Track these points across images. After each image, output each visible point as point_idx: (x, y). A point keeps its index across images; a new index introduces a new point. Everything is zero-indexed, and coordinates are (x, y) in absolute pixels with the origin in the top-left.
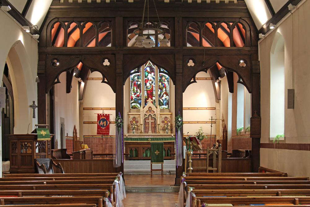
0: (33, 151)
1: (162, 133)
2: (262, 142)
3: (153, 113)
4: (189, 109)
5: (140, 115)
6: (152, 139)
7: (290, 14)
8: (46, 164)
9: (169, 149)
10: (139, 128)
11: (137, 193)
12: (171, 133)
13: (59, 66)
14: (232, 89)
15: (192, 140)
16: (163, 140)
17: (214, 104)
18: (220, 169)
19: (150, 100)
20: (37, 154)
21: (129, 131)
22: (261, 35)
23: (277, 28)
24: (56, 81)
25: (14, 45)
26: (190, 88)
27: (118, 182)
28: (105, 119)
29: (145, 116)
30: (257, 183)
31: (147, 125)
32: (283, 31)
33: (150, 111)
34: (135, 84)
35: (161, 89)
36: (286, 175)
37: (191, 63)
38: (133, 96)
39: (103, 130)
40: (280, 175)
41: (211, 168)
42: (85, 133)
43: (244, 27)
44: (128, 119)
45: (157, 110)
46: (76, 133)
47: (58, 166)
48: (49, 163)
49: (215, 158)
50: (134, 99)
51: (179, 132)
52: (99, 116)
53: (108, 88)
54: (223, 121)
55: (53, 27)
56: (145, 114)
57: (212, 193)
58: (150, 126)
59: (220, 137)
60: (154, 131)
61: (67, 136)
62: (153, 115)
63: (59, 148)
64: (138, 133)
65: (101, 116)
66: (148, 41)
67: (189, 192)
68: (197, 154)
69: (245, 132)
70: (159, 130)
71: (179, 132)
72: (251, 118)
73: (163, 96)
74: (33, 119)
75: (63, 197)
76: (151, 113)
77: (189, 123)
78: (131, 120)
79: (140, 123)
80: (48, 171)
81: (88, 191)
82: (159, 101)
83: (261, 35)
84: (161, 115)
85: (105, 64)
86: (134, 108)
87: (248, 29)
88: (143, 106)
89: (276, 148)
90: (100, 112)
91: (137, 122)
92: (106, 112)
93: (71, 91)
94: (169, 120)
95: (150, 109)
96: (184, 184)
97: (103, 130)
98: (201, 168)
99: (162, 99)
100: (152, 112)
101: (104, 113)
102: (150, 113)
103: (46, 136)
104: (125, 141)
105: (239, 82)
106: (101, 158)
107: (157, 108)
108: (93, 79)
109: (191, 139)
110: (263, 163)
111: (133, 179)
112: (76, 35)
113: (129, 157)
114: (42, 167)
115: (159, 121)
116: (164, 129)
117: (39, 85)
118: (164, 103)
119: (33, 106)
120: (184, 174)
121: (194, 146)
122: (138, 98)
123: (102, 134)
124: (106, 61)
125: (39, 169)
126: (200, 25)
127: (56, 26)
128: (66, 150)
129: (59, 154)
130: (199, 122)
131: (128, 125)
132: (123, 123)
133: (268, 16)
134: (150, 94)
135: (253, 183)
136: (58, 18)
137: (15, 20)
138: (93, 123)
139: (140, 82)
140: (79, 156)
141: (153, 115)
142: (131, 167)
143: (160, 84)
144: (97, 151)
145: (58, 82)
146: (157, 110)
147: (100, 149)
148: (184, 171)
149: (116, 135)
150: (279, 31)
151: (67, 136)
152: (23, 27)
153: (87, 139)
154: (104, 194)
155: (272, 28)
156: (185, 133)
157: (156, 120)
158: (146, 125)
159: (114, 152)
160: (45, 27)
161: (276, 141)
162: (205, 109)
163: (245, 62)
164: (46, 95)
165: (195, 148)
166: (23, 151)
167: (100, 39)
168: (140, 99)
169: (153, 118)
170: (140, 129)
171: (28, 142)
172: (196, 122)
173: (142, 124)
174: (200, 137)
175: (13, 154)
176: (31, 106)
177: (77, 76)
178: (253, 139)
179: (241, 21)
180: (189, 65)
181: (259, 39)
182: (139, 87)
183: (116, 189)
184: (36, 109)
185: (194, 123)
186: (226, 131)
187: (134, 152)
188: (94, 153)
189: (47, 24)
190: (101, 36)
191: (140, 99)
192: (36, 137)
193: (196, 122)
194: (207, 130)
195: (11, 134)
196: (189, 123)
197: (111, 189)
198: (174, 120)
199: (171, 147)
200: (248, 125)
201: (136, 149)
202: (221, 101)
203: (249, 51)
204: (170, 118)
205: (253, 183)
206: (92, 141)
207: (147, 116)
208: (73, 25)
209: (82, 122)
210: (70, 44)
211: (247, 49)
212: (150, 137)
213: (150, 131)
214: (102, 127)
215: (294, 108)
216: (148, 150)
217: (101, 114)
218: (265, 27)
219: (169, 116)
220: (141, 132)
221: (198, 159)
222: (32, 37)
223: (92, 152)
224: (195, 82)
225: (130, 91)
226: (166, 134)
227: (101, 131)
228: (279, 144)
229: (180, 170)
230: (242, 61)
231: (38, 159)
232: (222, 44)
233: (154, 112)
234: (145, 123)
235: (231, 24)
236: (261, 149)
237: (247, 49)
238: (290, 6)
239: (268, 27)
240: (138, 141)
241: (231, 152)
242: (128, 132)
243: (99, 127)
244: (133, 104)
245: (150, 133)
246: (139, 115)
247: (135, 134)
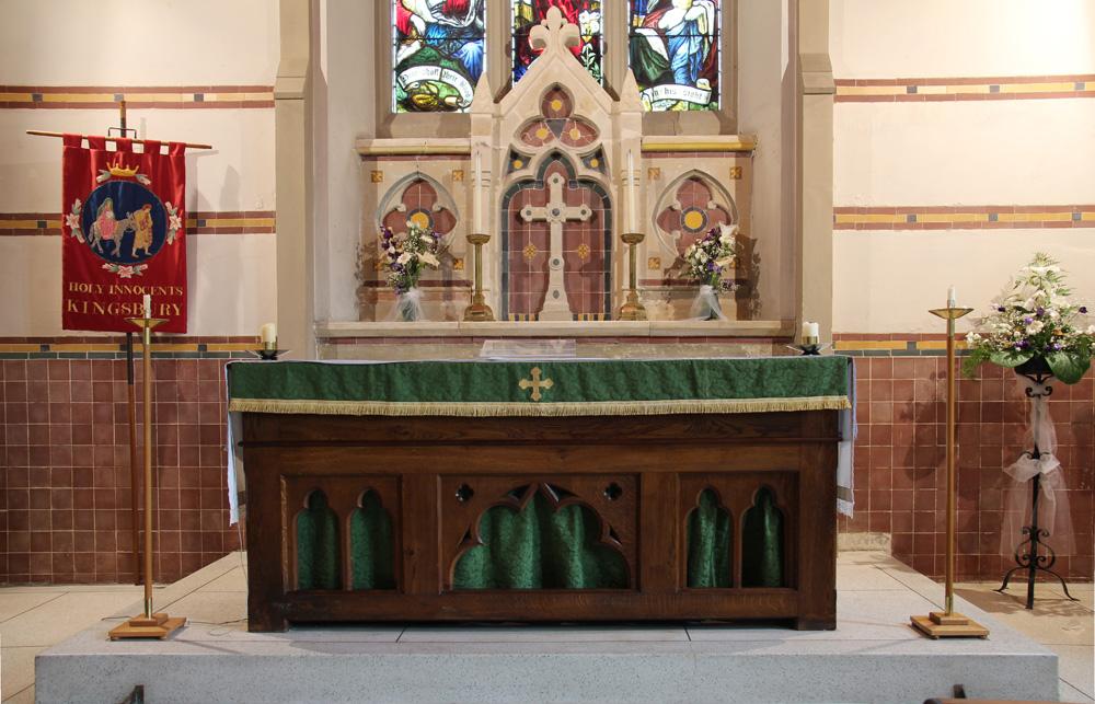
1: (658, 315)
3: (581, 143)
5: (466, 155)
9: (765, 493)
10: (461, 274)
16: (696, 396)
21: (374, 299)
28: (139, 187)
29: (511, 170)
31: (531, 252)
45: (614, 115)
50: (421, 27)
52: (79, 158)
56: (514, 155)
58: (556, 251)
60: (595, 298)
62: (586, 159)
64: (449, 318)
65: (105, 159)
70: (632, 286)
75: (285, 551)
76: (567, 140)
77: (912, 224)
78: (396, 202)
79: (469, 224)
82: (638, 45)
84: (656, 162)
88: (500, 84)
90: (99, 124)
91: (443, 221)
94: (719, 199)
95: (557, 105)
99: (662, 25)
100: (576, 134)
101: (130, 135)
102: (556, 144)
104: (239, 404)
107: (616, 98)
115: (632, 213)
116: (681, 284)
118: (675, 66)
122: (452, 22)
130: (1009, 210)
131: (366, 249)
141: (586, 159)
147: (109, 464)
157: (607, 204)
158: (519, 246)
162: (1071, 87)
168: (476, 34)
169: (586, 182)
170: (468, 284)
172: (977, 217)
173: (486, 239)
174: (1051, 350)
185: (958, 226)
187: (355, 531)
193: (977, 217)
199: (793, 478)
201: (371, 496)
204: (730, 185)
206: (39, 392)
207: (531, 171)
212: (559, 353)
214: (113, 259)
216: (515, 511)
217: (98, 143)
219: (719, 169)
220: (477, 311)
226: (697, 325)
227: (106, 299)
233: (590, 130)
234: (515, 228)
240: (390, 397)
243: (80, 262)
245: (557, 314)
246: (457, 163)
247: (422, 325)
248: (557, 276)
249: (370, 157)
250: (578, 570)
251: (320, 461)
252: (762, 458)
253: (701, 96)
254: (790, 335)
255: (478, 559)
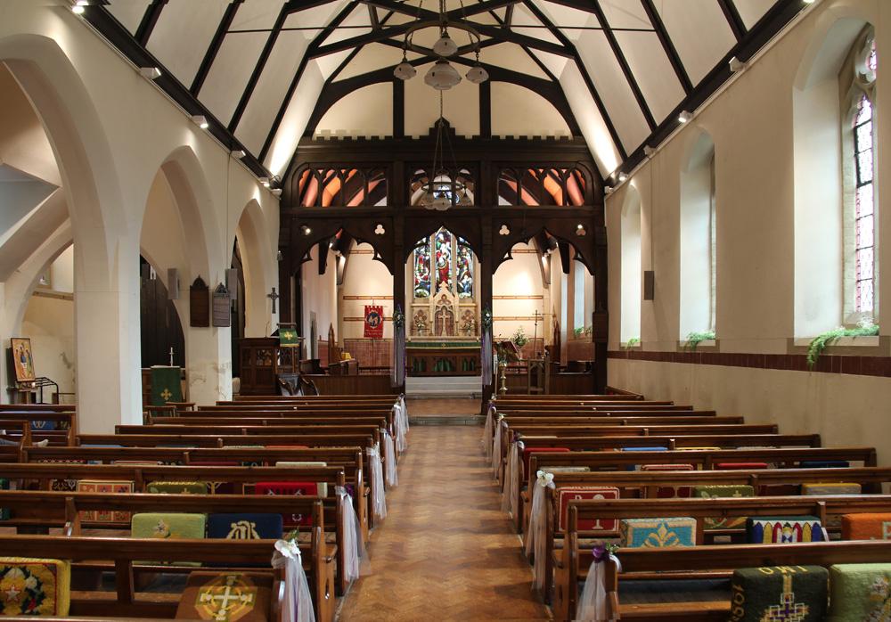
0: (274, 362)
1: (461, 335)
2: (610, 348)
4: (503, 297)
6: (447, 345)
7: (647, 160)
8: (293, 381)
9: (472, 360)
11: (426, 425)
12: (476, 335)
13: (310, 235)
14: (567, 269)
15: (506, 348)
17: (541, 291)
18: (547, 390)
19: (443, 285)
20: (279, 368)
22: (608, 189)
23: (630, 179)
24: (306, 257)
25: (248, 206)
26: (503, 268)
27: (399, 408)
30: (598, 409)
31: (440, 324)
32: (642, 186)
33: (444, 302)
34: (421, 260)
35: (461, 267)
36: (642, 398)
37: (504, 231)
38: (419, 277)
39: (374, 330)
40: (634, 398)
41: (533, 389)
42: (347, 335)
43: (583, 176)
44: (412, 315)
46: (333, 335)
47: (310, 385)
48: (296, 380)
49: (539, 372)
51: (487, 334)
52: (367, 309)
53: (382, 268)
54: (554, 316)
55: (301, 177)
57: (531, 422)
59: (549, 341)
61: (320, 340)
63: (309, 358)
66: (441, 201)
67: (499, 420)
68: (515, 367)
69: (586, 334)
71: (487, 334)
72: (594, 314)
73: (463, 278)
74: (273, 315)
80: (296, 392)
81: (331, 446)
82: (458, 285)
83: (608, 189)
85: (377, 232)
86: (420, 296)
87: (589, 178)
89: (630, 358)
90: (370, 303)
91: (425, 318)
92: (378, 303)
93: (326, 271)
96: (493, 410)
97: (374, 330)
98: (520, 388)
103: (292, 341)
105: (576, 258)
106: (370, 374)
108: (358, 252)
109: (506, 345)
110: (613, 382)
111: (418, 405)
112: (334, 186)
113: (413, 372)
114: (287, 387)
115: (457, 318)
116: (465, 330)
117: (280, 263)
119: (272, 296)
120: (493, 397)
121: (509, 356)
123: (372, 336)
124: (380, 227)
125: (283, 390)
126: (518, 173)
127: (305, 175)
128: (318, 361)
129: (309, 367)
132: (404, 320)
133: (618, 161)
134: (444, 275)
135: (591, 409)
136: (309, 163)
137: (249, 169)
138: (358, 319)
139: (430, 256)
140: (339, 370)
142: (416, 387)
143: (460, 259)
144: (364, 363)
145: (309, 259)
146: (455, 300)
148: (494, 392)
149: (873, 279)
150: (633, 183)
151: (320, 340)
152: (259, 179)
153: (350, 345)
154: (380, 423)
155: (622, 179)
156: (496, 333)
159: (391, 365)
160: (290, 177)
161: (629, 348)
163: (585, 228)
164: (292, 278)
165: (511, 358)
166: (260, 362)
167: (370, 189)
171: (266, 350)
175: (245, 368)
176: (269, 296)
177: (334, 249)
178: (596, 345)
179: (579, 166)
180: (502, 232)
181: (605, 194)
182: (427, 263)
183: (396, 417)
184: (277, 300)
186: (559, 333)
188: (360, 365)
189: (292, 172)
190: (371, 185)
191: (429, 283)
192: (278, 341)
194: (530, 330)
195: (241, 338)
196: (503, 319)
197: (390, 417)
198: (480, 315)
199: (475, 357)
200: (590, 324)
201: (423, 360)
202: (552, 286)
203: (591, 212)
205: (591, 409)
208: (330, 173)
209: (342, 319)
210: (325, 203)
211: (588, 208)
212: (445, 341)
213: (444, 333)
215: (653, 299)
218: (613, 176)
219: (472, 309)
221: (516, 375)
222: (271, 193)
223: (358, 364)
224: (510, 258)
225: (413, 270)
226: (467, 337)
228: (633, 352)
229: (487, 391)
230: (580, 227)
231: (281, 374)
232: (552, 200)
233: (450, 302)
234: (437, 319)
235: (564, 171)
236: (608, 360)
237: (588, 208)
238: (647, 149)
239: (617, 177)
241: (566, 364)
242: (412, 335)
243: (367, 326)
244: (418, 291)
247: (422, 337)
248: (444, 328)
249: (412, 307)
250: (449, 369)
251: (417, 355)
252: (472, 354)
253: (469, 295)
254: (364, 308)
255: (436, 368)
